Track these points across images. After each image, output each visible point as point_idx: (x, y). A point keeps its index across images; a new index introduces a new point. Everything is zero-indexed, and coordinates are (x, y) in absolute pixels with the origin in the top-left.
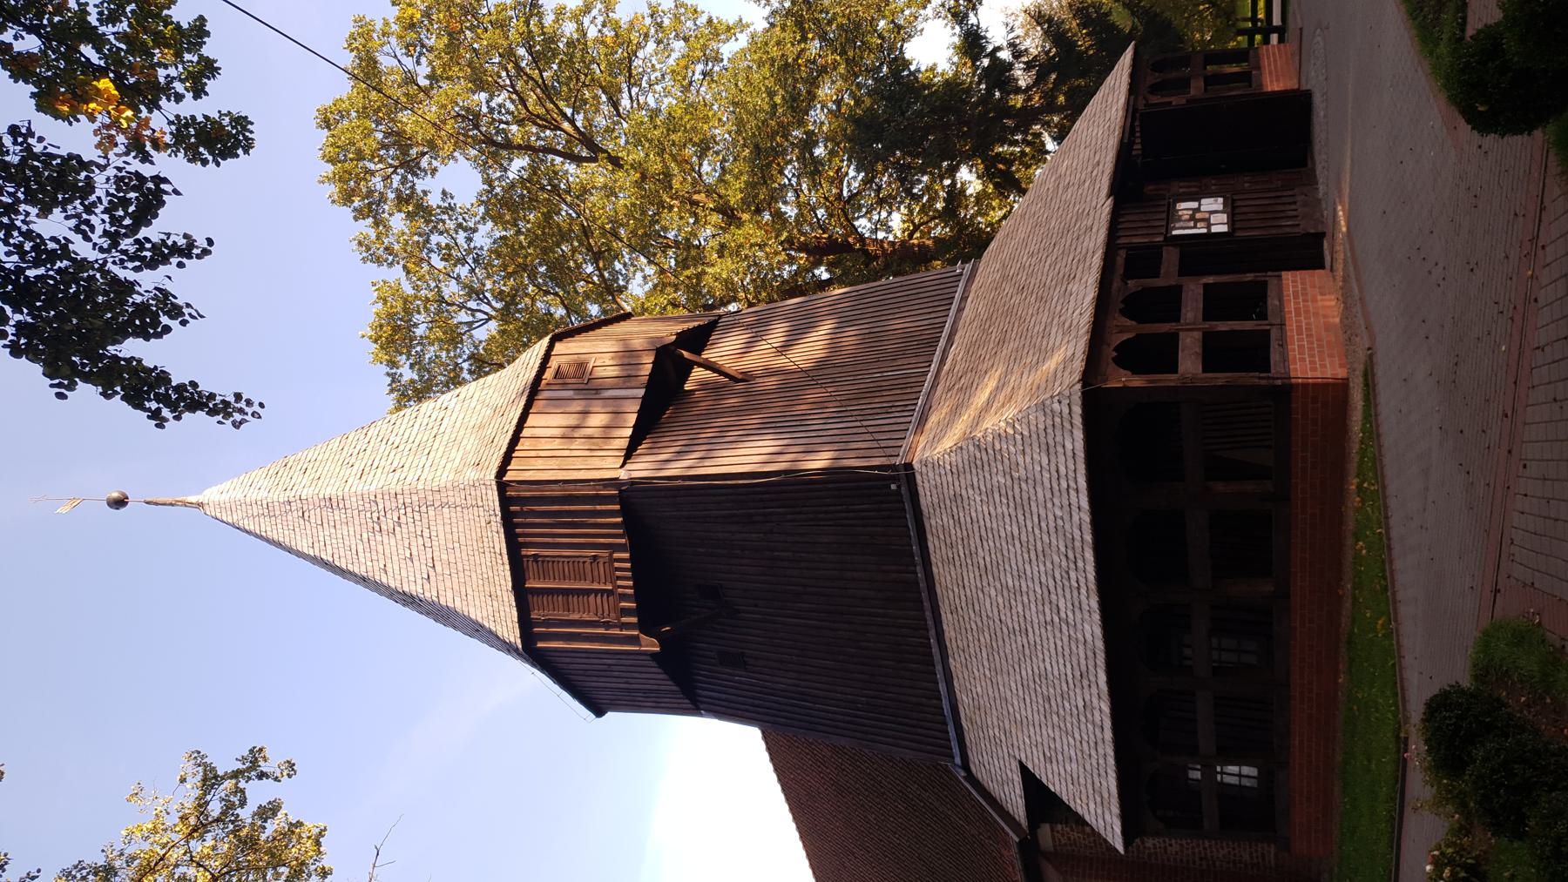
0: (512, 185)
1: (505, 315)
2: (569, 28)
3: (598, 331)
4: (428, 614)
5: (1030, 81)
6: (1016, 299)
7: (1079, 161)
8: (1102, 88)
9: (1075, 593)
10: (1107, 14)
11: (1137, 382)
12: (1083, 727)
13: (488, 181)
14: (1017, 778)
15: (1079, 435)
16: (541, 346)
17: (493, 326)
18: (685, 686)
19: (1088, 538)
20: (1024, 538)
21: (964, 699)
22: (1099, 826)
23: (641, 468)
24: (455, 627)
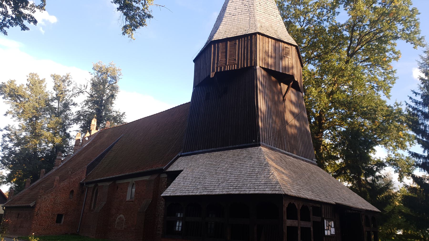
0: (341, 32)
1: (303, 31)
2: (388, 47)
3: (298, 58)
4: (220, 14)
5: (369, 181)
6: (306, 176)
7: (342, 191)
8: (367, 202)
9: (227, 188)
10: (390, 204)
11: (285, 209)
12: (192, 187)
13: (342, 26)
14: (179, 169)
15: (270, 192)
16: (295, 43)
17: (299, 27)
18: (201, 84)
19: (242, 193)
20: (241, 175)
21: (198, 156)
22: (168, 190)
23: (260, 73)
24: (217, 21)
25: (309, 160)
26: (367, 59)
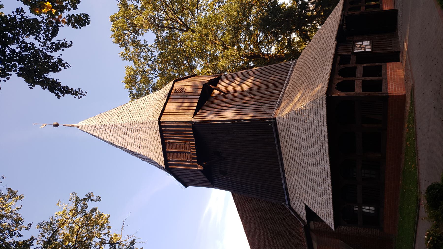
1: (162, 75)
3: (187, 79)
4: (139, 158)
6: (308, 71)
9: (322, 156)
11: (342, 94)
12: (323, 194)
13: (158, 37)
14: (304, 208)
15: (325, 110)
18: (210, 179)
19: (327, 140)
20: (308, 140)
21: (289, 186)
22: (327, 222)
23: (198, 118)
25: (291, 68)
26: (192, 13)
